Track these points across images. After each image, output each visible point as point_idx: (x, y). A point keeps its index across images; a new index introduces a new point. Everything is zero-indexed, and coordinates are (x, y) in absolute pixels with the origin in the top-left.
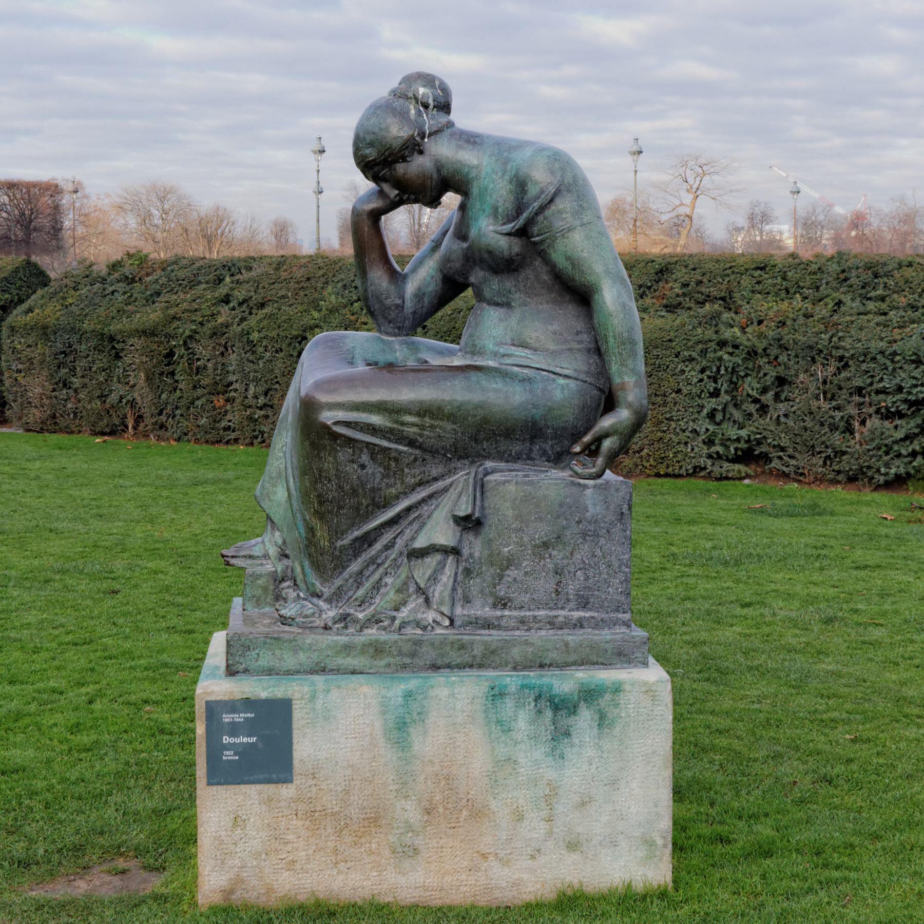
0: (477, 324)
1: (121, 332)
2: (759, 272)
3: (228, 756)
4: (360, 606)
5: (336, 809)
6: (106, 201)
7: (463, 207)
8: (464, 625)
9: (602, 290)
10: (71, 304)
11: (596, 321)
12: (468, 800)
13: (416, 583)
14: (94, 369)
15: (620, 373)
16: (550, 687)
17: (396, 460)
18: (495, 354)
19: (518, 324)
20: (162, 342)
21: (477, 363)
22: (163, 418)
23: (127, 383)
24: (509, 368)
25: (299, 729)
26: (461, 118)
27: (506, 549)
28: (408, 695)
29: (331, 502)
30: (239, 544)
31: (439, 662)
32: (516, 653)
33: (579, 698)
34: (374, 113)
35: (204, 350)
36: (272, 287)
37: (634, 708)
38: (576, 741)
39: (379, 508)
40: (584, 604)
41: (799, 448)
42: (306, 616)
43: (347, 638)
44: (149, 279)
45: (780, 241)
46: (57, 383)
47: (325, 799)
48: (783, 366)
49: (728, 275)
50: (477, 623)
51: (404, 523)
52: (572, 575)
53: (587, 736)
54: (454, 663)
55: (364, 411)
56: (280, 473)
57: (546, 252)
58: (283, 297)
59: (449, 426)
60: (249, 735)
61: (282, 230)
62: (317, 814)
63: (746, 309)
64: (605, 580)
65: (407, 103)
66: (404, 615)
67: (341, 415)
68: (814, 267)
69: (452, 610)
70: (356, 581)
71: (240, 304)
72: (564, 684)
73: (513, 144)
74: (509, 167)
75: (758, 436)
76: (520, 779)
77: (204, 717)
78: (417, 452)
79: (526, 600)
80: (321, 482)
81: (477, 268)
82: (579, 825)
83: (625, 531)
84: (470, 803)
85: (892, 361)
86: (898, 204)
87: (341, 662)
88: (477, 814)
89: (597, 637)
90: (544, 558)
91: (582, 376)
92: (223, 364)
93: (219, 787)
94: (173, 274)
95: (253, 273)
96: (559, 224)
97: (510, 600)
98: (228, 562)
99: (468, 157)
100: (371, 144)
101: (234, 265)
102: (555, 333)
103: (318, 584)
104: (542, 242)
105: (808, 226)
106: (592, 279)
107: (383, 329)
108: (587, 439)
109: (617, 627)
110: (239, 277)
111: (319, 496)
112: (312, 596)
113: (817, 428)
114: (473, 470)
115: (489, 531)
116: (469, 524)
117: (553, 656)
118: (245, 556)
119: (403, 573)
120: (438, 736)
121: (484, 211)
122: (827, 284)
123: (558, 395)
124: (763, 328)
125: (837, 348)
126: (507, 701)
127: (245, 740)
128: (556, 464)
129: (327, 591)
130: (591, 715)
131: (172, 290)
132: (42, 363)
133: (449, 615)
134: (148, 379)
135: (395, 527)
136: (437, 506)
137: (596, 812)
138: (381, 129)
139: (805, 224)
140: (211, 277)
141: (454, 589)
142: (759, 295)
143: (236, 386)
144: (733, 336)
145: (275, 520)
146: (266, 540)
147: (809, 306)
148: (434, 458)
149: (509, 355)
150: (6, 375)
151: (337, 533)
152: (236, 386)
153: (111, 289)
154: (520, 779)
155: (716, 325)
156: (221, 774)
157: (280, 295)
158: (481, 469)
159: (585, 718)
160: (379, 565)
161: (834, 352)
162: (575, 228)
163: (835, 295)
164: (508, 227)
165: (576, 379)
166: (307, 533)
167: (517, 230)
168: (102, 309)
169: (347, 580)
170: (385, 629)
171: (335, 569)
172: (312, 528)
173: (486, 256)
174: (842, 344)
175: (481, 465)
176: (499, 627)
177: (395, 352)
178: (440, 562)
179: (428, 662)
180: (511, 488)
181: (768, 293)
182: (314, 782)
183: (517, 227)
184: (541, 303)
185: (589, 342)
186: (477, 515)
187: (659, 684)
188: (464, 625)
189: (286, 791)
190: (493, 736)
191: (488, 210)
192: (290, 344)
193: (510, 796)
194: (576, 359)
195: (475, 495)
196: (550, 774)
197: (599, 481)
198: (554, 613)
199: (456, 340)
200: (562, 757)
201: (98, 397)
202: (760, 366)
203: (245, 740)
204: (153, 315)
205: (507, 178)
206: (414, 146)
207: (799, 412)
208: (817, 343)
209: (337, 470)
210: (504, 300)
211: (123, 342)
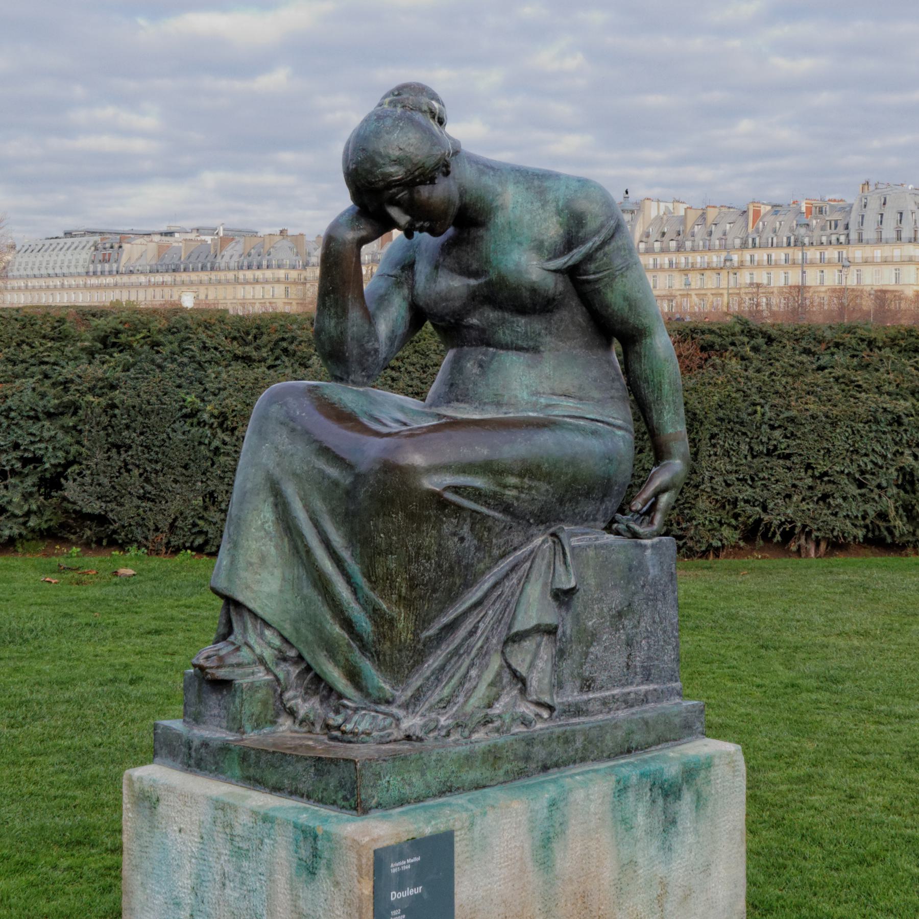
16: (661, 771)
24: (560, 419)
25: (459, 867)
27: (590, 623)
28: (553, 804)
29: (426, 585)
31: (549, 763)
33: (683, 779)
40: (647, 679)
59: (544, 486)
60: (415, 886)
67: (449, 480)
78: (509, 519)
80: (417, 562)
85: (7, 417)
103: (387, 687)
104: (597, 281)
106: (646, 321)
116: (564, 597)
117: (637, 738)
135: (479, 608)
145: (267, 617)
148: (519, 524)
151: (424, 622)
159: (685, 805)
170: (497, 730)
171: (413, 666)
179: (540, 764)
183: (570, 263)
184: (575, 348)
198: (627, 690)
200: (670, 849)
209: (440, 545)
210: (531, 344)
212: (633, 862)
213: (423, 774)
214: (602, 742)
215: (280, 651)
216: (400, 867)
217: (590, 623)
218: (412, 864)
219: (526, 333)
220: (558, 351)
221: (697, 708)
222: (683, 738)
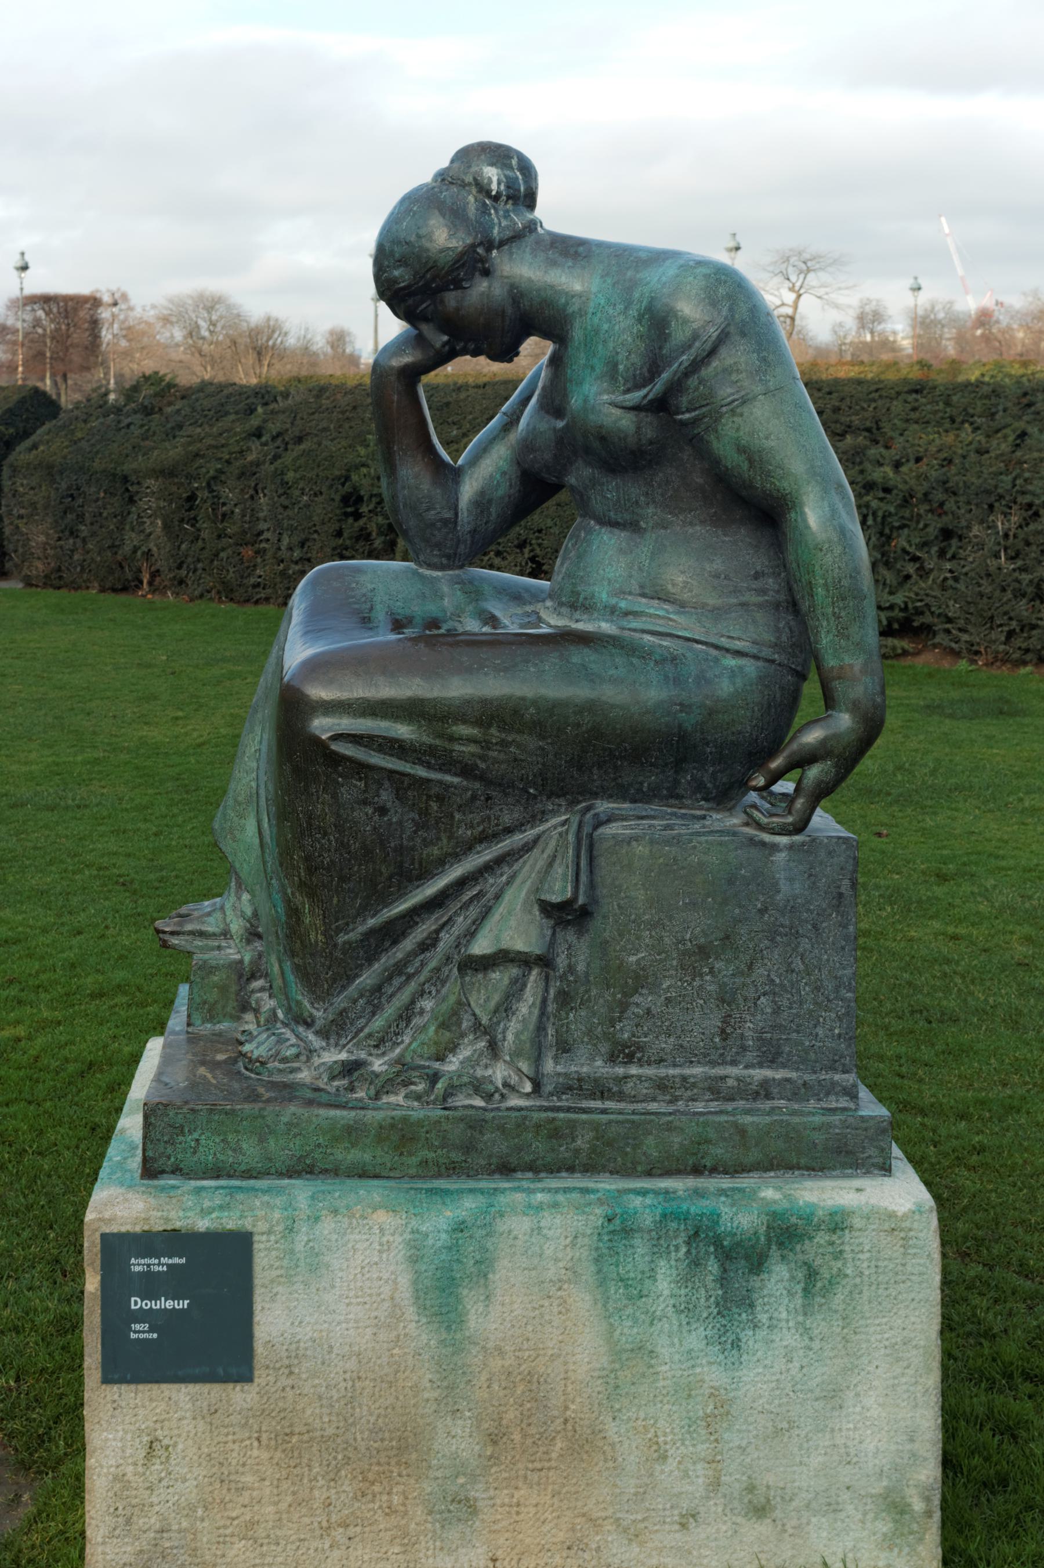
0: (580, 557)
1: (135, 471)
2: (914, 396)
3: (140, 1332)
4: (377, 1046)
5: (330, 1431)
6: (152, 313)
7: (556, 361)
9: (802, 505)
10: (80, 440)
12: (566, 1421)
13: (474, 1014)
14: (105, 515)
16: (715, 1218)
17: (440, 799)
18: (612, 611)
19: (652, 559)
20: (182, 484)
22: (183, 572)
23: (142, 531)
24: (637, 635)
25: (264, 1286)
26: (556, 210)
27: (633, 959)
28: (460, 1227)
29: (328, 869)
30: (184, 910)
31: (514, 1161)
33: (769, 1240)
34: (408, 211)
35: (229, 493)
37: (870, 1260)
38: (763, 1318)
39: (410, 881)
40: (771, 1057)
41: (973, 619)
42: (285, 1060)
43: (353, 1113)
45: (895, 342)
47: (309, 1412)
48: (950, 516)
49: (875, 401)
50: (581, 1088)
51: (454, 906)
53: (782, 1309)
54: (539, 1162)
55: (384, 717)
57: (702, 439)
58: (325, 429)
61: (339, 340)
62: (294, 1440)
63: (899, 442)
64: (810, 1011)
65: (464, 193)
66: (452, 1068)
67: (346, 724)
68: (986, 390)
69: (537, 1067)
70: (369, 1002)
71: (274, 438)
72: (747, 1203)
73: (643, 255)
75: (919, 604)
76: (661, 1384)
77: (98, 1262)
78: (477, 785)
79: (668, 1047)
81: (580, 463)
82: (768, 1470)
83: (845, 927)
84: (569, 1427)
86: (1030, 299)
87: (340, 1157)
88: (582, 1447)
89: (796, 1120)
90: (701, 975)
91: (766, 652)
93: (124, 1387)
95: (290, 401)
96: (725, 392)
97: (640, 1048)
98: (165, 941)
99: (570, 282)
100: (403, 262)
102: (717, 576)
103: (306, 1003)
105: (925, 324)
106: (785, 485)
108: (775, 764)
109: (833, 1098)
111: (307, 859)
112: (297, 1023)
113: (997, 593)
114: (575, 820)
115: (603, 926)
116: (567, 915)
117: (718, 1152)
118: (191, 933)
119: (451, 990)
120: (512, 1303)
121: (593, 368)
122: (1005, 410)
123: (725, 688)
124: (923, 467)
125: (1023, 493)
126: (637, 1242)
127: (169, 1304)
129: (320, 1015)
130: (790, 1270)
132: (46, 507)
134: (166, 526)
137: (801, 1448)
138: (419, 236)
141: (540, 1028)
142: (916, 426)
146: (228, 906)
147: (980, 437)
148: (506, 795)
149: (636, 614)
150: (6, 521)
154: (661, 1384)
155: (861, 463)
156: (127, 1366)
159: (778, 1279)
160: (410, 977)
161: (1019, 499)
162: (755, 398)
163: (1016, 424)
164: (635, 397)
165: (756, 657)
166: (289, 917)
167: (651, 401)
168: (115, 445)
169: (355, 1002)
170: (418, 1097)
172: (297, 909)
173: (596, 444)
174: (1030, 487)
175: (588, 809)
176: (621, 1096)
177: (442, 598)
179: (494, 1160)
180: (640, 849)
181: (928, 422)
182: (290, 1382)
183: (650, 397)
184: (691, 524)
185: (778, 592)
186: (581, 900)
187: (917, 1217)
189: (240, 1397)
190: (611, 1306)
191: (600, 368)
192: (331, 487)
193: (642, 1415)
194: (754, 622)
195: (578, 865)
196: (714, 1376)
197: (797, 838)
198: (719, 1071)
199: (538, 571)
200: (736, 1344)
202: (919, 515)
203: (169, 1304)
204: (173, 451)
205: (633, 312)
206: (473, 263)
207: (972, 574)
208: (996, 487)
209: (338, 816)
210: (627, 516)
211: (139, 483)
212: (644, 1351)
213: (262, 1140)
215: (252, 925)
216: (149, 1265)
217: (633, 959)
218: (168, 1265)
219: (618, 500)
220: (666, 528)
221: (872, 1123)
222: (834, 1168)
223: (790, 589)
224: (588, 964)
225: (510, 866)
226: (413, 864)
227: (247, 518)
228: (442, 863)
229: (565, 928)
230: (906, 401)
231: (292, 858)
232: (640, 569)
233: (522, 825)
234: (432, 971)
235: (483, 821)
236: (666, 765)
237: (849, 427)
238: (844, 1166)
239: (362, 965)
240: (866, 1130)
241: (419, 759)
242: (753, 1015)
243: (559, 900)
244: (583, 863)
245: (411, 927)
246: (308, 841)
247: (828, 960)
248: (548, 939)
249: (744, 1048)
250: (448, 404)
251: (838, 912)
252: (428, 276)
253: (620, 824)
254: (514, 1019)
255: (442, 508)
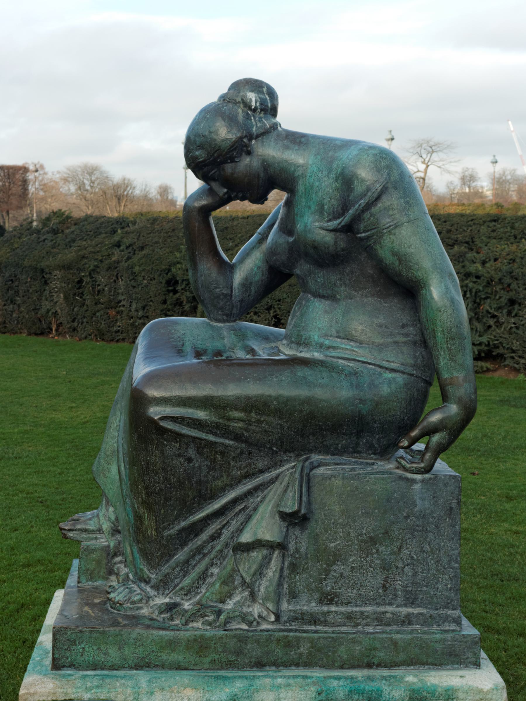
0: (302, 315)
1: (48, 266)
2: (494, 223)
4: (186, 595)
6: (58, 176)
7: (289, 204)
8: (291, 620)
9: (429, 285)
10: (16, 248)
11: (423, 316)
13: (242, 576)
14: (31, 291)
15: (448, 368)
17: (222, 453)
20: (75, 274)
21: (302, 355)
22: (75, 324)
23: (52, 301)
24: (335, 360)
26: (288, 118)
27: (333, 545)
29: (158, 494)
30: (76, 517)
31: (265, 660)
32: (343, 651)
34: (204, 117)
35: (101, 279)
36: (149, 235)
39: (205, 500)
40: (412, 600)
42: (133, 602)
44: (67, 231)
45: (482, 192)
46: (6, 301)
48: (514, 292)
49: (471, 226)
52: (400, 571)
54: (279, 661)
55: (191, 406)
56: (114, 452)
57: (372, 248)
58: (157, 242)
59: (275, 421)
63: (485, 250)
64: (434, 575)
65: (236, 107)
69: (278, 606)
70: (182, 570)
71: (127, 248)
73: (338, 143)
74: (335, 166)
75: (496, 342)
78: (243, 445)
81: (302, 261)
83: (454, 526)
87: (165, 658)
89: (426, 636)
90: (372, 554)
91: (409, 370)
92: (115, 289)
94: (84, 228)
96: (385, 221)
97: (337, 596)
98: (65, 535)
99: (296, 158)
100: (201, 147)
101: (124, 221)
103: (146, 570)
104: (368, 238)
106: (420, 274)
107: (212, 316)
109: (447, 624)
110: (127, 229)
111: (146, 487)
112: (141, 581)
115: (316, 526)
116: (295, 520)
117: (381, 655)
119: (229, 563)
121: (310, 207)
123: (385, 390)
124: (498, 264)
128: (381, 457)
131: (83, 238)
133: (274, 611)
134: (66, 298)
136: (263, 499)
138: (210, 132)
139: (498, 182)
140: (109, 229)
141: (280, 584)
142: (494, 241)
143: (123, 303)
144: (476, 270)
146: (101, 514)
148: (260, 451)
149: (334, 348)
152: (123, 303)
153: (43, 238)
155: (463, 262)
157: (154, 241)
158: (307, 463)
160: (205, 555)
162: (402, 224)
164: (334, 224)
165: (403, 372)
166: (136, 521)
167: (343, 227)
168: (37, 251)
169: (174, 569)
170: (210, 624)
171: (162, 557)
173: (312, 251)
175: (307, 459)
176: (325, 623)
177: (223, 339)
178: (266, 557)
179: (253, 660)
180: (337, 482)
181: (501, 238)
183: (342, 224)
184: (366, 296)
186: (303, 511)
187: (495, 692)
188: (291, 620)
191: (313, 207)
192: (160, 275)
194: (402, 352)
195: (301, 491)
197: (427, 476)
201: (33, 310)
204: (70, 255)
205: (333, 176)
206: (241, 147)
209: (164, 463)
210: (329, 292)
211: (50, 273)
214: (334, 652)
215: (115, 526)
217: (333, 545)
219: (324, 283)
220: (351, 299)
223: (422, 334)
224: (307, 548)
225: (263, 492)
226: (207, 490)
227: (112, 293)
228: (223, 490)
229: (294, 527)
230: (489, 226)
231: (138, 487)
232: (337, 322)
233: (269, 468)
234: (218, 552)
235: (247, 466)
236: (352, 434)
237: (456, 241)
238: (454, 663)
239: (178, 548)
240: (466, 642)
241: (210, 431)
242: (401, 577)
243: (290, 511)
244: (304, 490)
245: (206, 527)
246: (147, 478)
247: (444, 546)
248: (284, 533)
249: (396, 596)
250: (227, 228)
251: (450, 518)
252: (216, 155)
253: (325, 468)
254: (265, 579)
255: (224, 287)
